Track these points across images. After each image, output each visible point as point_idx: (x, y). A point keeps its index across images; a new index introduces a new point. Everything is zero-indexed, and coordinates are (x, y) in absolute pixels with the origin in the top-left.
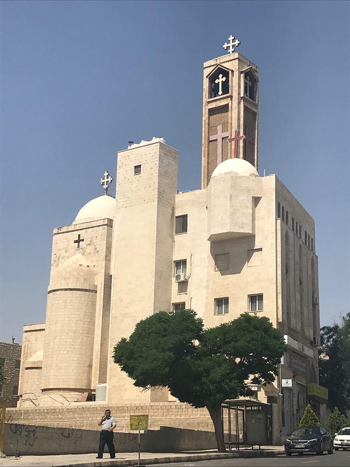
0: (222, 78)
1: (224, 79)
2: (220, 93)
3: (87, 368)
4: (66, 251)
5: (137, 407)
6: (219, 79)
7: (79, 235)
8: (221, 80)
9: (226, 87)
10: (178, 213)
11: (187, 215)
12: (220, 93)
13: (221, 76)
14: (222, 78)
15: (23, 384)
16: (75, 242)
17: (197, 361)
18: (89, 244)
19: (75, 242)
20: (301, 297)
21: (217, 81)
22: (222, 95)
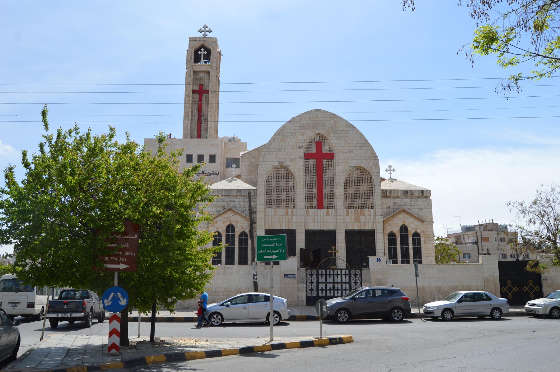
8: (203, 52)
21: (199, 53)
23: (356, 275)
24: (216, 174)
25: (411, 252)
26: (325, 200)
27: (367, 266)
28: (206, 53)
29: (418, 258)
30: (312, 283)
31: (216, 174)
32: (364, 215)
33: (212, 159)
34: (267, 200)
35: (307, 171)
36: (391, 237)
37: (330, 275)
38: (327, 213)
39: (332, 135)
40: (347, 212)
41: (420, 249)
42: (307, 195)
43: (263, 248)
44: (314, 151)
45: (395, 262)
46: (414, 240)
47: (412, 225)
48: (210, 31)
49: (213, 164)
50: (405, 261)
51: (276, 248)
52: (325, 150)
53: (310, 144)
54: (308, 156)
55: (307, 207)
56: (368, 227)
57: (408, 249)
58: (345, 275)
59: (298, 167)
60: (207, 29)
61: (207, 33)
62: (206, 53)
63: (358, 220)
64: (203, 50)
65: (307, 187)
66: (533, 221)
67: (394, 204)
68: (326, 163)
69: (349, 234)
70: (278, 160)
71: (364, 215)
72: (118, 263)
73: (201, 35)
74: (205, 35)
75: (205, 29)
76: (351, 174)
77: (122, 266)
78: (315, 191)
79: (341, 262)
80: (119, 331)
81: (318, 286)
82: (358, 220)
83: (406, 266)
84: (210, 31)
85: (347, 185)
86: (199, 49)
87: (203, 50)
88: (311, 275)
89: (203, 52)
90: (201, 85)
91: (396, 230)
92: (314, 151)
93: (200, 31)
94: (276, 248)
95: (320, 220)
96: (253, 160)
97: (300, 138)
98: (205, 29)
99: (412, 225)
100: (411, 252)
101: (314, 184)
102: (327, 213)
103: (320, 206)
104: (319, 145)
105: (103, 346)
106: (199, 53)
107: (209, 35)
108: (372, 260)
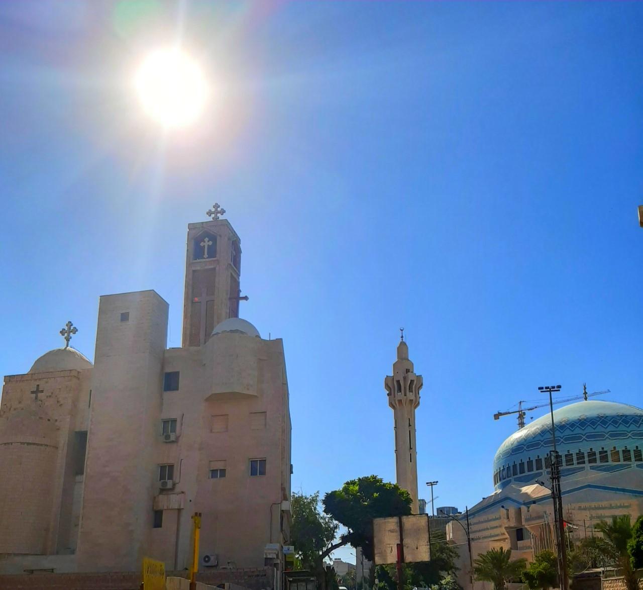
0: (208, 241)
1: (211, 243)
2: (206, 255)
3: (486, 527)
4: (20, 402)
5: (124, 576)
6: (205, 242)
7: (38, 385)
8: (207, 243)
9: (212, 252)
10: (169, 370)
11: (178, 372)
12: (206, 255)
13: (206, 239)
14: (208, 241)
15: (536, 517)
16: (33, 392)
17: (329, 564)
18: (50, 396)
19: (33, 392)
20: (620, 507)
21: (202, 244)
22: (207, 258)
28: (211, 243)
34: (87, 435)
48: (223, 212)
60: (219, 209)
61: (219, 215)
66: (59, 404)
69: (257, 475)
73: (210, 219)
74: (216, 219)
75: (217, 210)
79: (219, 476)
80: (93, 362)
84: (223, 212)
93: (209, 213)
98: (217, 210)
105: (239, 291)
106: (202, 244)
107: (221, 217)
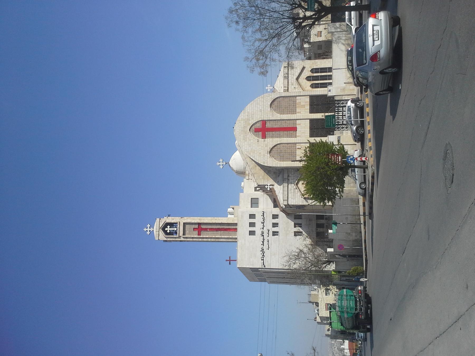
8: (168, 229)
21: (168, 231)
23: (338, 104)
24: (263, 214)
25: (323, 74)
26: (291, 126)
27: (333, 97)
28: (168, 227)
29: (330, 69)
30: (343, 128)
31: (263, 214)
32: (300, 102)
33: (252, 216)
35: (272, 137)
36: (313, 86)
37: (338, 109)
38: (299, 124)
39: (250, 122)
40: (299, 112)
41: (321, 69)
42: (288, 136)
43: (330, 124)
44: (260, 133)
45: (330, 84)
46: (316, 73)
47: (306, 74)
49: (256, 216)
50: (330, 77)
51: (330, 119)
52: (259, 126)
53: (256, 136)
54: (264, 137)
55: (296, 137)
56: (308, 99)
57: (321, 76)
58: (338, 114)
59: (271, 141)
62: (168, 227)
63: (303, 106)
64: (166, 229)
65: (283, 137)
67: (292, 85)
68: (268, 125)
70: (266, 154)
71: (300, 102)
72: (339, 159)
76: (275, 110)
77: (340, 158)
78: (286, 132)
81: (344, 124)
82: (303, 106)
83: (334, 77)
85: (282, 113)
86: (166, 232)
87: (166, 229)
88: (338, 128)
89: (168, 229)
90: (194, 229)
91: (309, 83)
92: (260, 133)
94: (330, 119)
95: (304, 129)
96: (261, 177)
97: (252, 141)
99: (306, 74)
100: (323, 74)
101: (282, 133)
102: (299, 124)
103: (295, 129)
104: (257, 130)
106: (168, 231)
108: (330, 94)
